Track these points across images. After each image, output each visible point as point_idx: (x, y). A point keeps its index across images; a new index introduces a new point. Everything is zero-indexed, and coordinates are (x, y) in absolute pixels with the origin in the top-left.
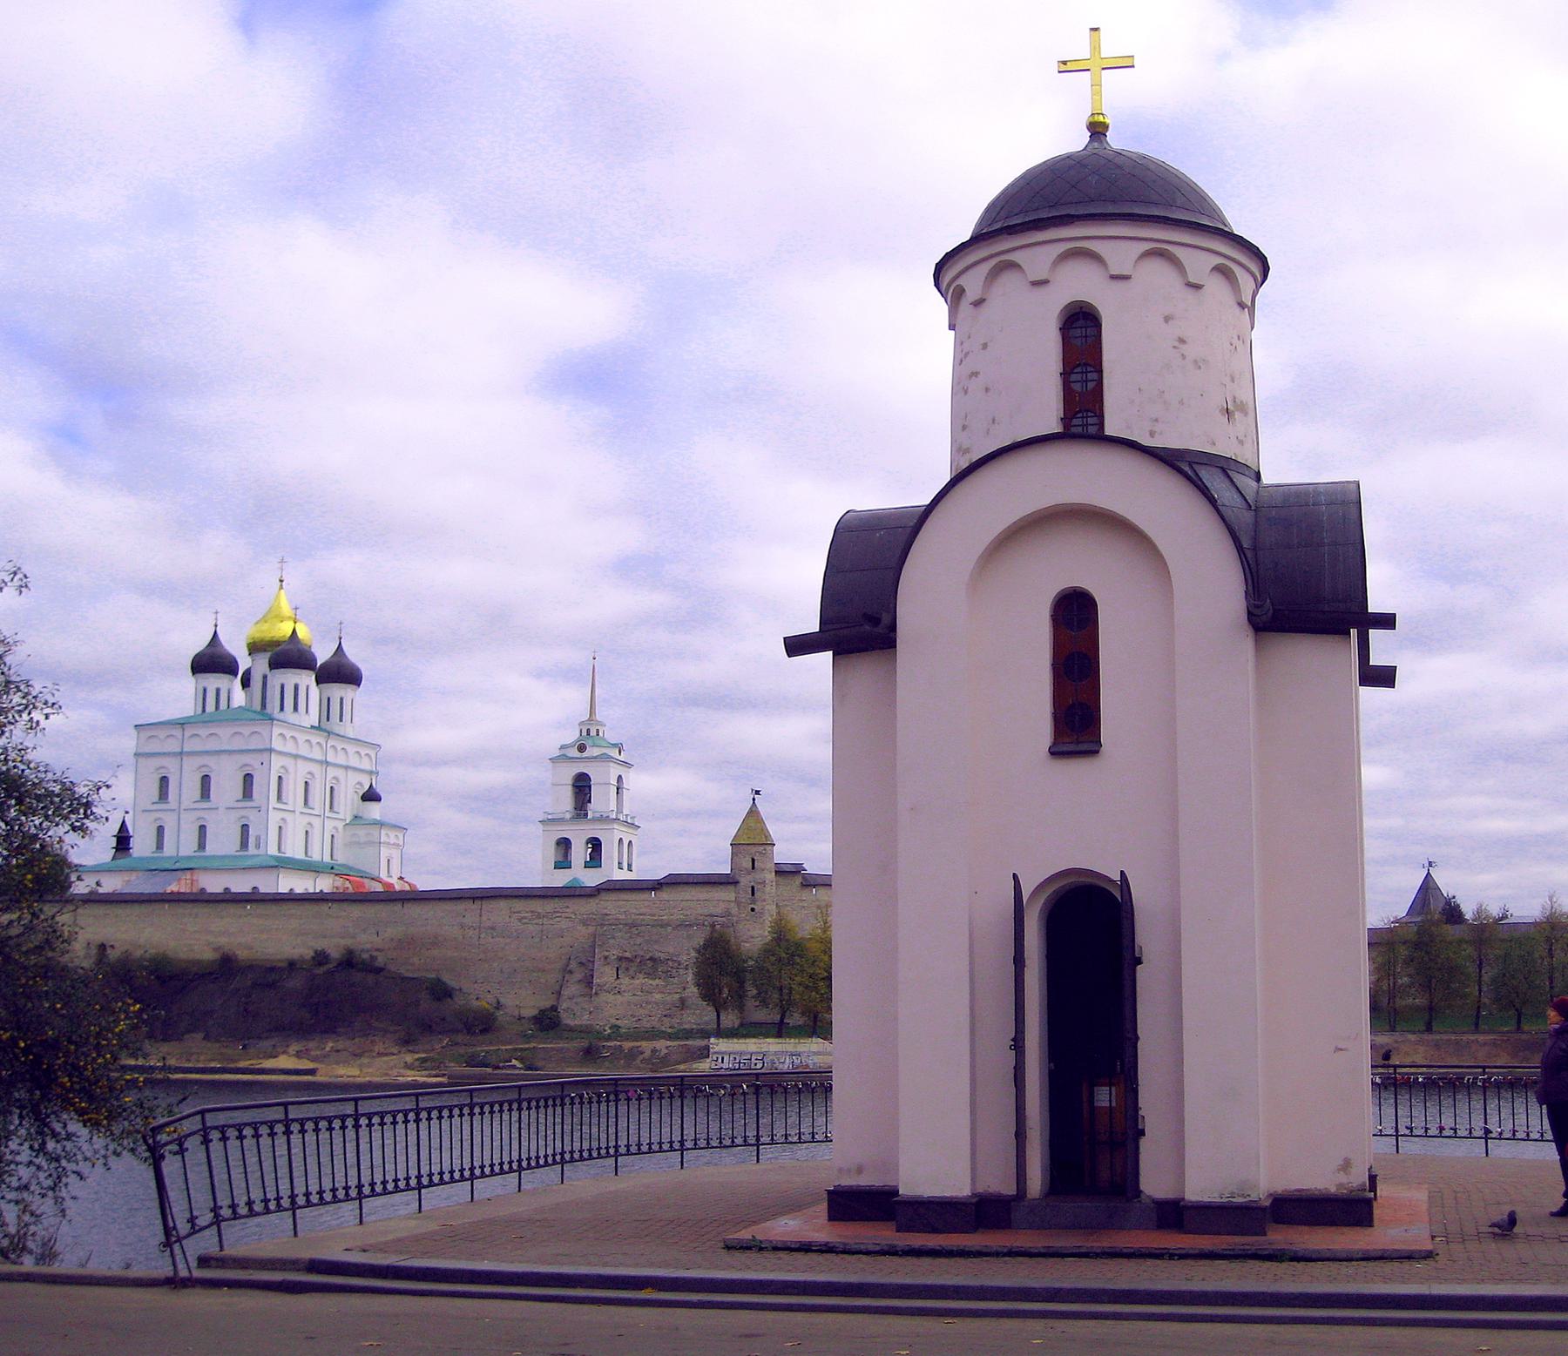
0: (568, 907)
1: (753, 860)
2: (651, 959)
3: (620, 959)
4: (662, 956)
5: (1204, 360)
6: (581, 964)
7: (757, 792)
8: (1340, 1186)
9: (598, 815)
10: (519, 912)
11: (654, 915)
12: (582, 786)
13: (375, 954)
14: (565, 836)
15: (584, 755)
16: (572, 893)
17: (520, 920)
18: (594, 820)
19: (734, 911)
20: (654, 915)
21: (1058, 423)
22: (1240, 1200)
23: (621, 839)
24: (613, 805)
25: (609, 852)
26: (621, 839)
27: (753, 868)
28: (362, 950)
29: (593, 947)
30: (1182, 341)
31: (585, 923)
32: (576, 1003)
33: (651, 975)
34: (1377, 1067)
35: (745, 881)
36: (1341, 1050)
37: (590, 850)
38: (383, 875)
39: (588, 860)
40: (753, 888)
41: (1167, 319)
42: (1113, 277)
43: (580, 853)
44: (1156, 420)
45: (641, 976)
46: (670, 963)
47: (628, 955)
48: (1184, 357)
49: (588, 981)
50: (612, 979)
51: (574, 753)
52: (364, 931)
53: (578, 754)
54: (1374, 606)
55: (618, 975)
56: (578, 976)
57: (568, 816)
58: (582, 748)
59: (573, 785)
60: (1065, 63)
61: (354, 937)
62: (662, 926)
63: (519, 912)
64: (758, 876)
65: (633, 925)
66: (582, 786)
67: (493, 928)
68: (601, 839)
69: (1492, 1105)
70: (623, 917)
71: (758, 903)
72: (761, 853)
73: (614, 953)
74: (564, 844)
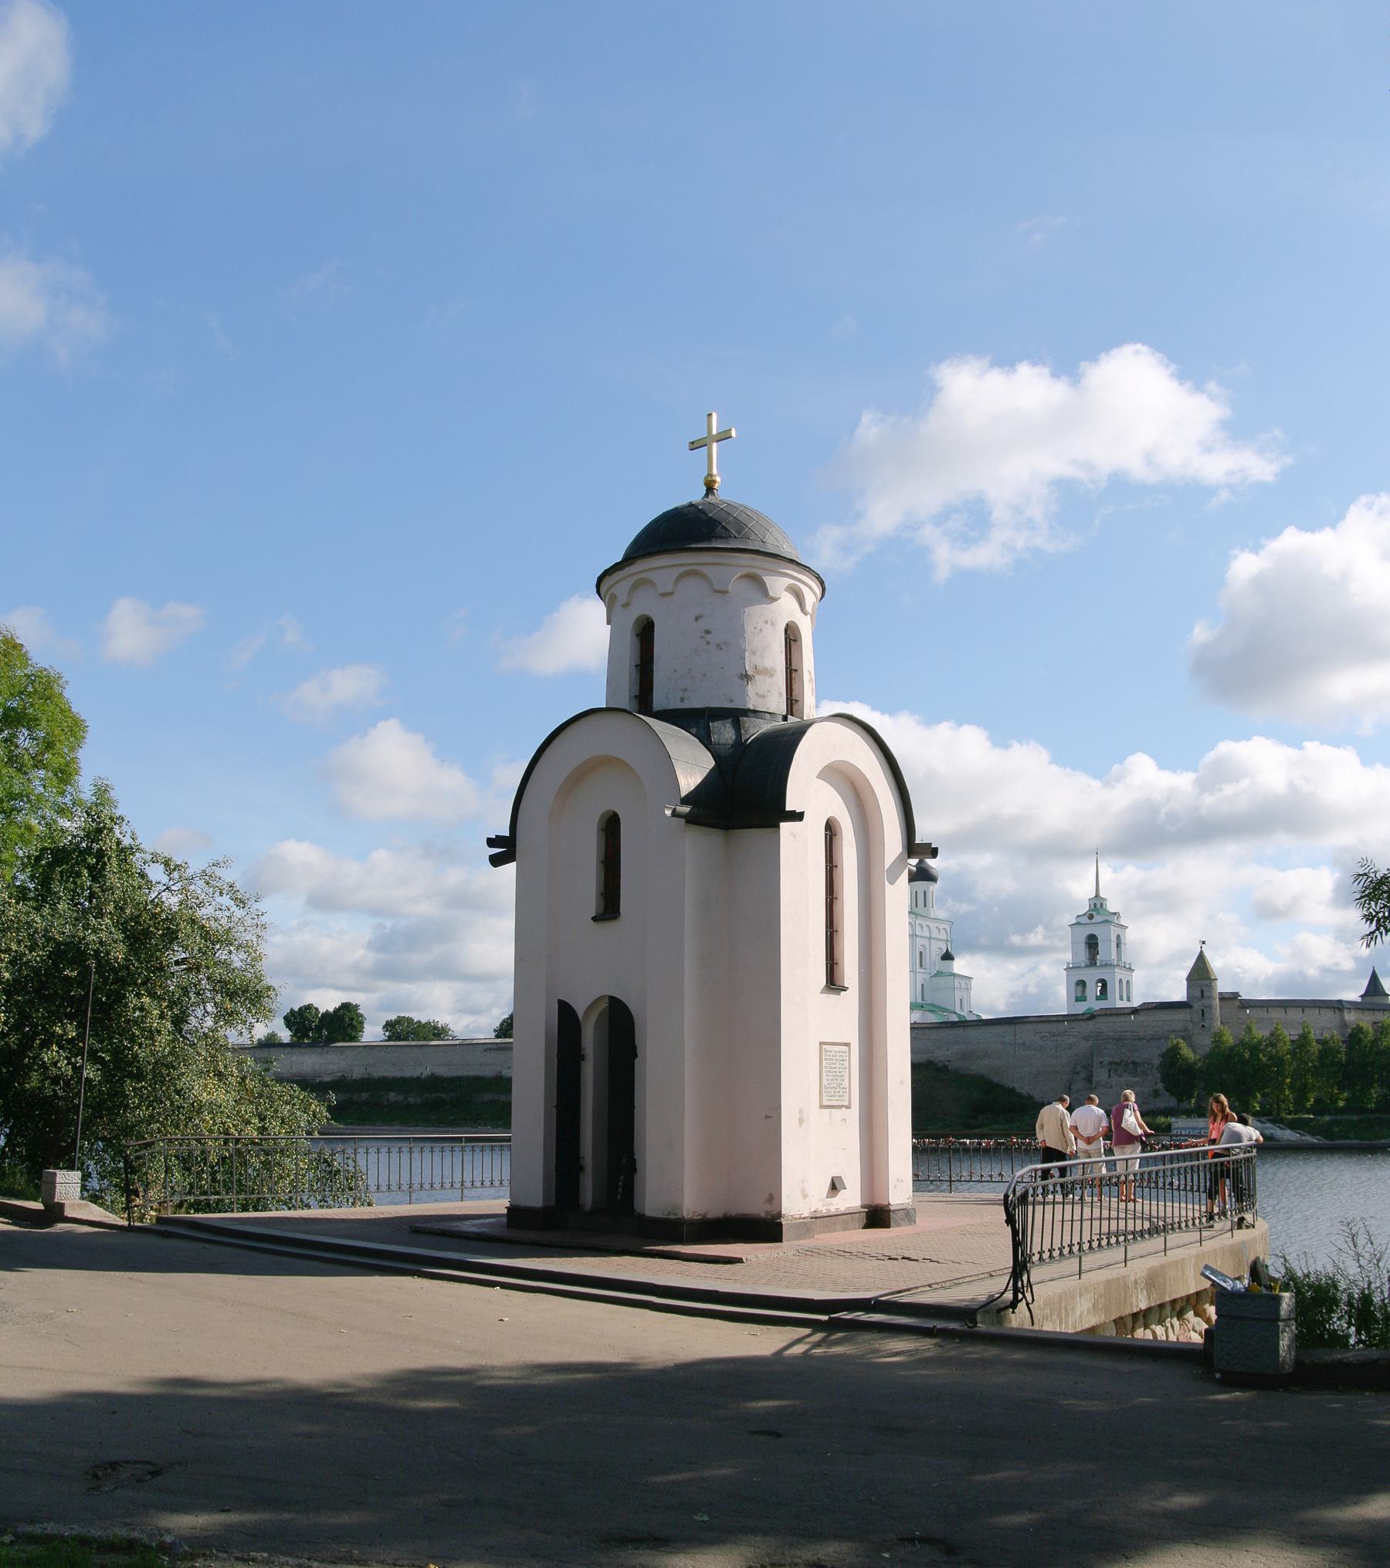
0: (1073, 1028)
1: (1202, 991)
2: (1132, 1062)
3: (1111, 1063)
4: (1140, 1060)
5: (725, 643)
6: (1084, 1067)
7: (1204, 942)
8: (767, 1212)
9: (1103, 963)
10: (1041, 1033)
11: (1134, 1032)
12: (1092, 943)
13: (947, 1063)
14: (1081, 979)
15: (1093, 921)
16: (1091, 1016)
17: (1042, 1038)
18: (1101, 966)
19: (1190, 1027)
20: (1134, 1032)
21: (630, 699)
22: (672, 1217)
23: (1121, 980)
24: (1114, 956)
25: (1114, 989)
26: (1121, 980)
27: (1202, 996)
28: (939, 1061)
29: (1092, 1055)
30: (708, 632)
31: (1086, 1039)
32: (1082, 1095)
33: (1134, 1074)
34: (1233, 1163)
35: (1197, 1006)
36: (769, 1117)
37: (1099, 988)
38: (958, 1011)
39: (1098, 994)
40: (1203, 1011)
41: (697, 619)
42: (662, 595)
43: (1093, 990)
44: (686, 690)
45: (1126, 1075)
46: (1146, 1065)
47: (1116, 1060)
48: (708, 643)
49: (1089, 1079)
50: (1106, 1078)
51: (1085, 920)
52: (939, 1048)
53: (1088, 921)
54: (790, 806)
55: (1109, 1075)
56: (1082, 1076)
57: (1083, 965)
58: (1091, 917)
59: (1086, 943)
60: (693, 443)
61: (932, 1053)
62: (1139, 1040)
63: (1041, 1033)
64: (1205, 1002)
65: (1119, 1039)
66: (1092, 943)
67: (1023, 1044)
68: (1107, 980)
69: (416, 1155)
70: (1112, 1034)
71: (1207, 1021)
72: (1207, 986)
73: (1107, 1059)
74: (1082, 984)
